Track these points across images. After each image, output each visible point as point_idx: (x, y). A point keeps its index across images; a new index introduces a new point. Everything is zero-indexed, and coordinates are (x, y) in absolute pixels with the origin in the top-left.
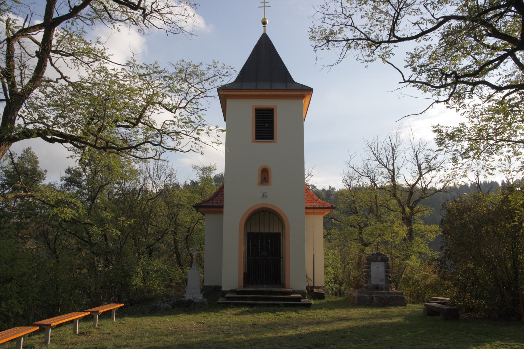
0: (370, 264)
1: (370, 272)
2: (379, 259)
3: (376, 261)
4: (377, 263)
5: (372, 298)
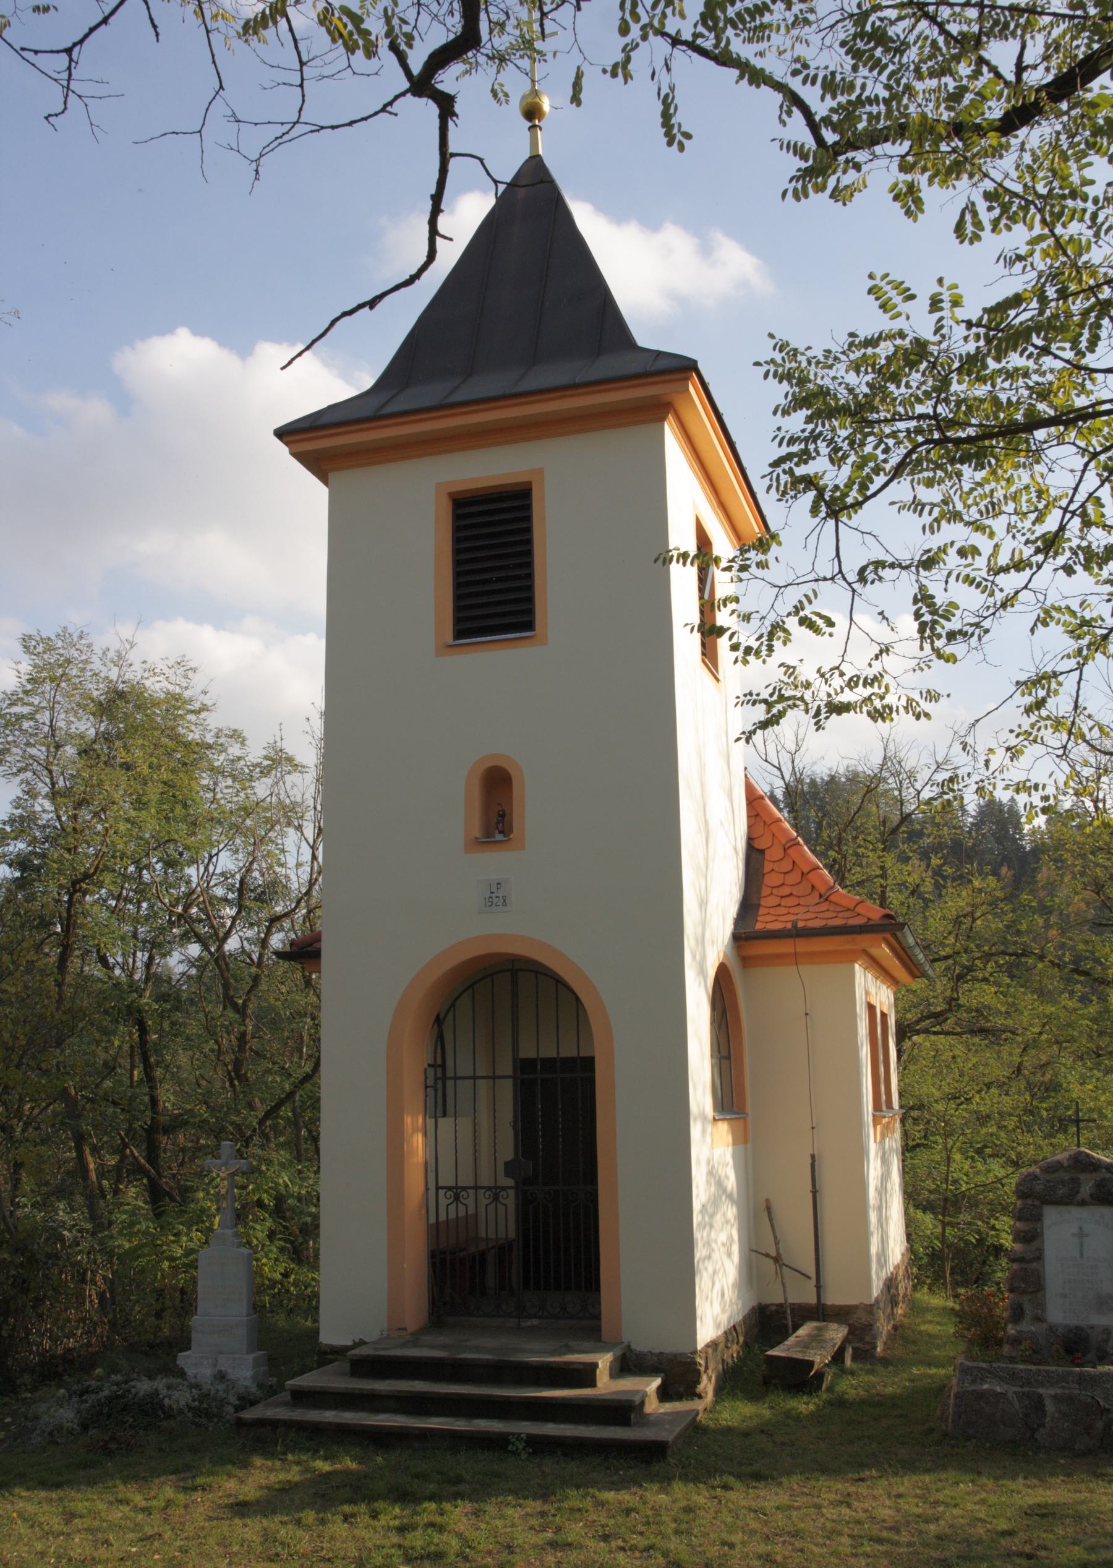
0: (1038, 1218)
1: (1039, 1257)
2: (1086, 1189)
3: (1069, 1200)
4: (1076, 1212)
5: (1038, 1404)
